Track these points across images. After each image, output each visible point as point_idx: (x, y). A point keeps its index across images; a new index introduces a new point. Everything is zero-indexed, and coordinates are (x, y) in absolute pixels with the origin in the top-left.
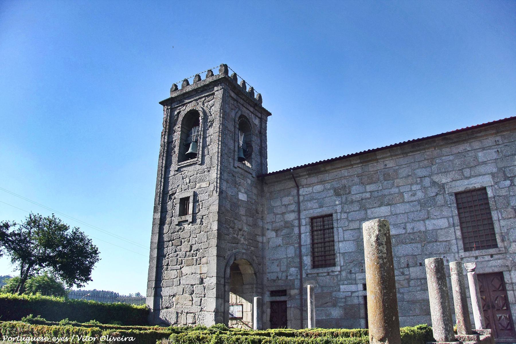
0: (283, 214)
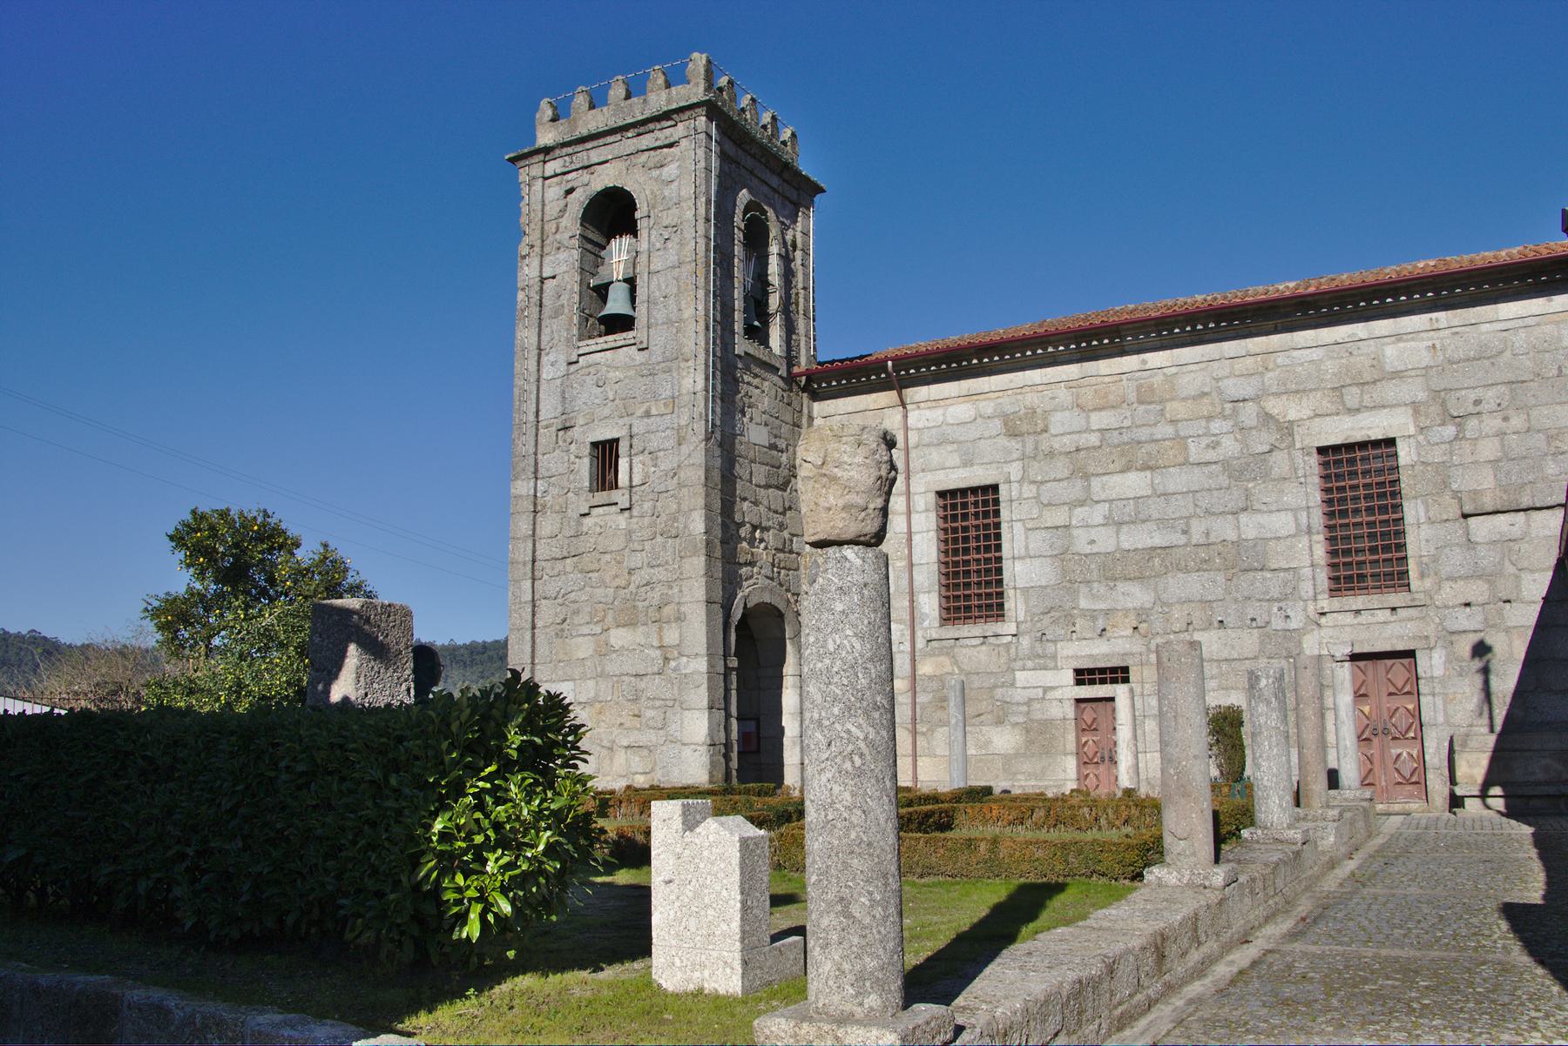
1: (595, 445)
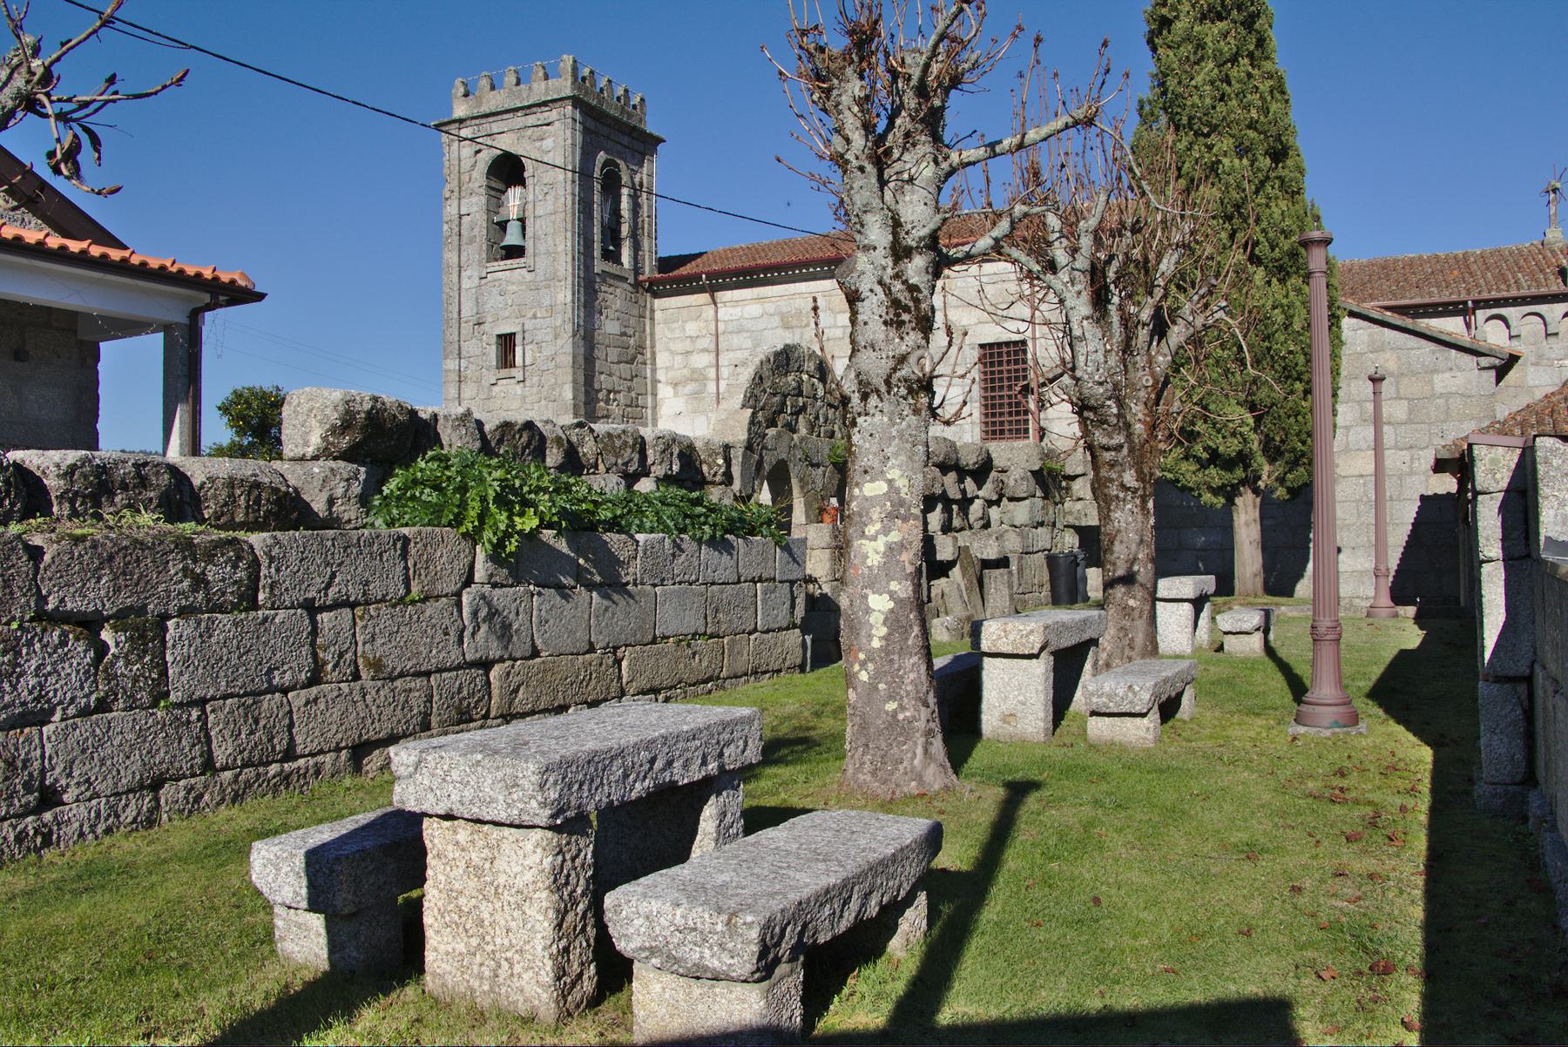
0: (688, 353)
1: (499, 336)
